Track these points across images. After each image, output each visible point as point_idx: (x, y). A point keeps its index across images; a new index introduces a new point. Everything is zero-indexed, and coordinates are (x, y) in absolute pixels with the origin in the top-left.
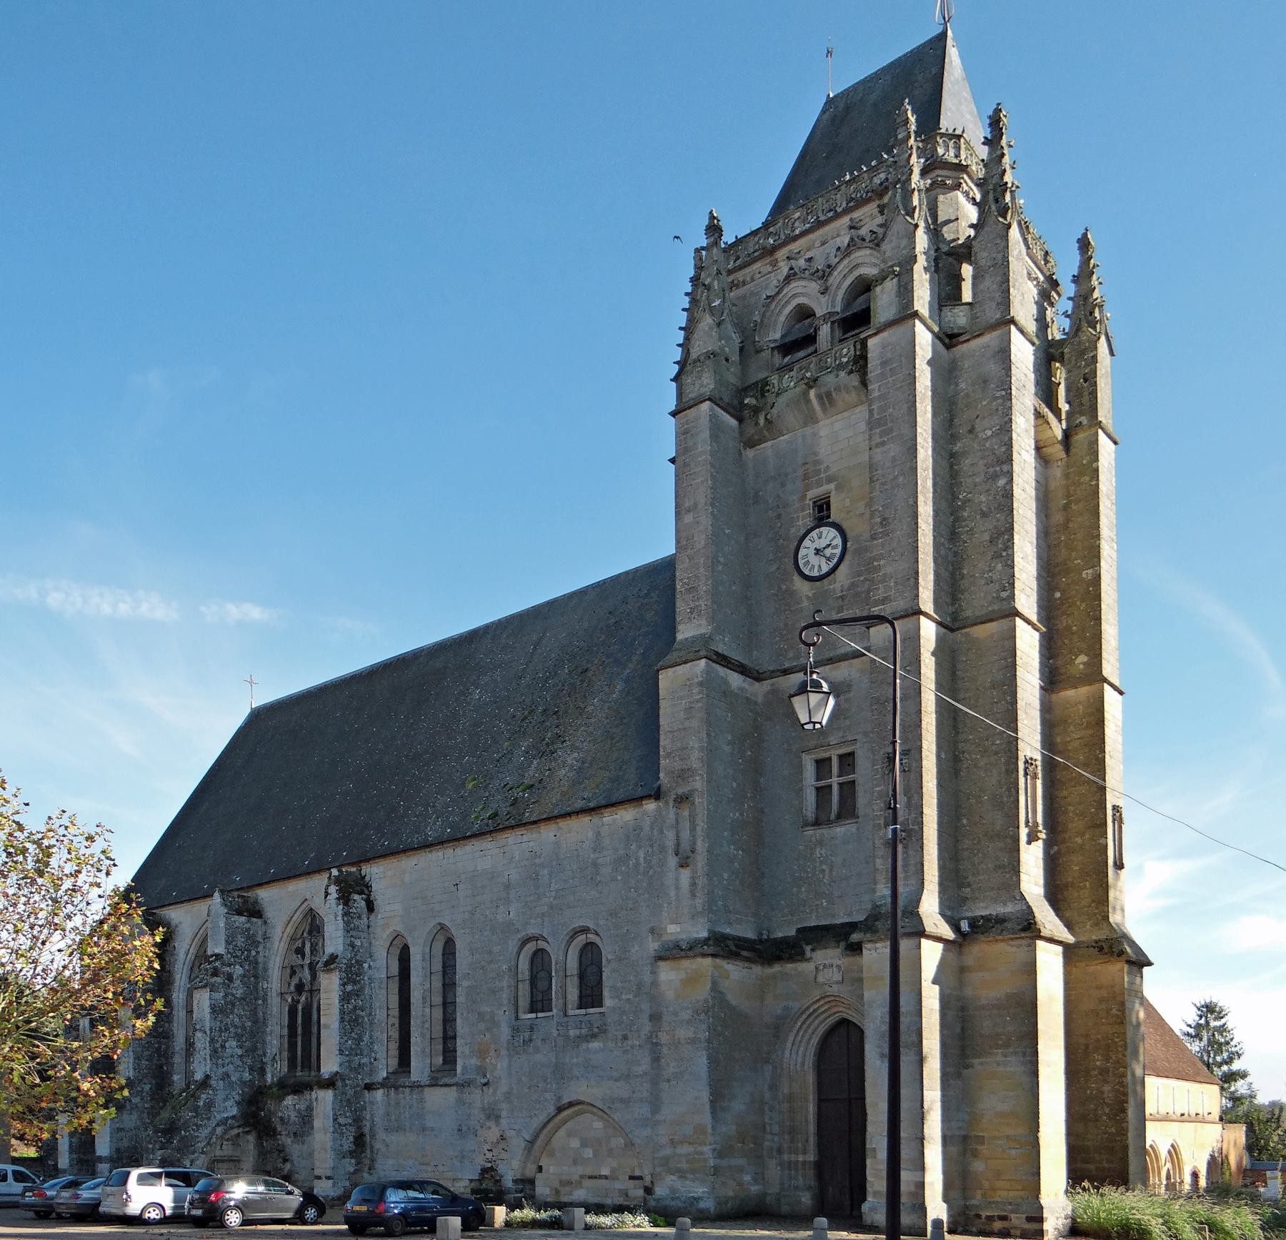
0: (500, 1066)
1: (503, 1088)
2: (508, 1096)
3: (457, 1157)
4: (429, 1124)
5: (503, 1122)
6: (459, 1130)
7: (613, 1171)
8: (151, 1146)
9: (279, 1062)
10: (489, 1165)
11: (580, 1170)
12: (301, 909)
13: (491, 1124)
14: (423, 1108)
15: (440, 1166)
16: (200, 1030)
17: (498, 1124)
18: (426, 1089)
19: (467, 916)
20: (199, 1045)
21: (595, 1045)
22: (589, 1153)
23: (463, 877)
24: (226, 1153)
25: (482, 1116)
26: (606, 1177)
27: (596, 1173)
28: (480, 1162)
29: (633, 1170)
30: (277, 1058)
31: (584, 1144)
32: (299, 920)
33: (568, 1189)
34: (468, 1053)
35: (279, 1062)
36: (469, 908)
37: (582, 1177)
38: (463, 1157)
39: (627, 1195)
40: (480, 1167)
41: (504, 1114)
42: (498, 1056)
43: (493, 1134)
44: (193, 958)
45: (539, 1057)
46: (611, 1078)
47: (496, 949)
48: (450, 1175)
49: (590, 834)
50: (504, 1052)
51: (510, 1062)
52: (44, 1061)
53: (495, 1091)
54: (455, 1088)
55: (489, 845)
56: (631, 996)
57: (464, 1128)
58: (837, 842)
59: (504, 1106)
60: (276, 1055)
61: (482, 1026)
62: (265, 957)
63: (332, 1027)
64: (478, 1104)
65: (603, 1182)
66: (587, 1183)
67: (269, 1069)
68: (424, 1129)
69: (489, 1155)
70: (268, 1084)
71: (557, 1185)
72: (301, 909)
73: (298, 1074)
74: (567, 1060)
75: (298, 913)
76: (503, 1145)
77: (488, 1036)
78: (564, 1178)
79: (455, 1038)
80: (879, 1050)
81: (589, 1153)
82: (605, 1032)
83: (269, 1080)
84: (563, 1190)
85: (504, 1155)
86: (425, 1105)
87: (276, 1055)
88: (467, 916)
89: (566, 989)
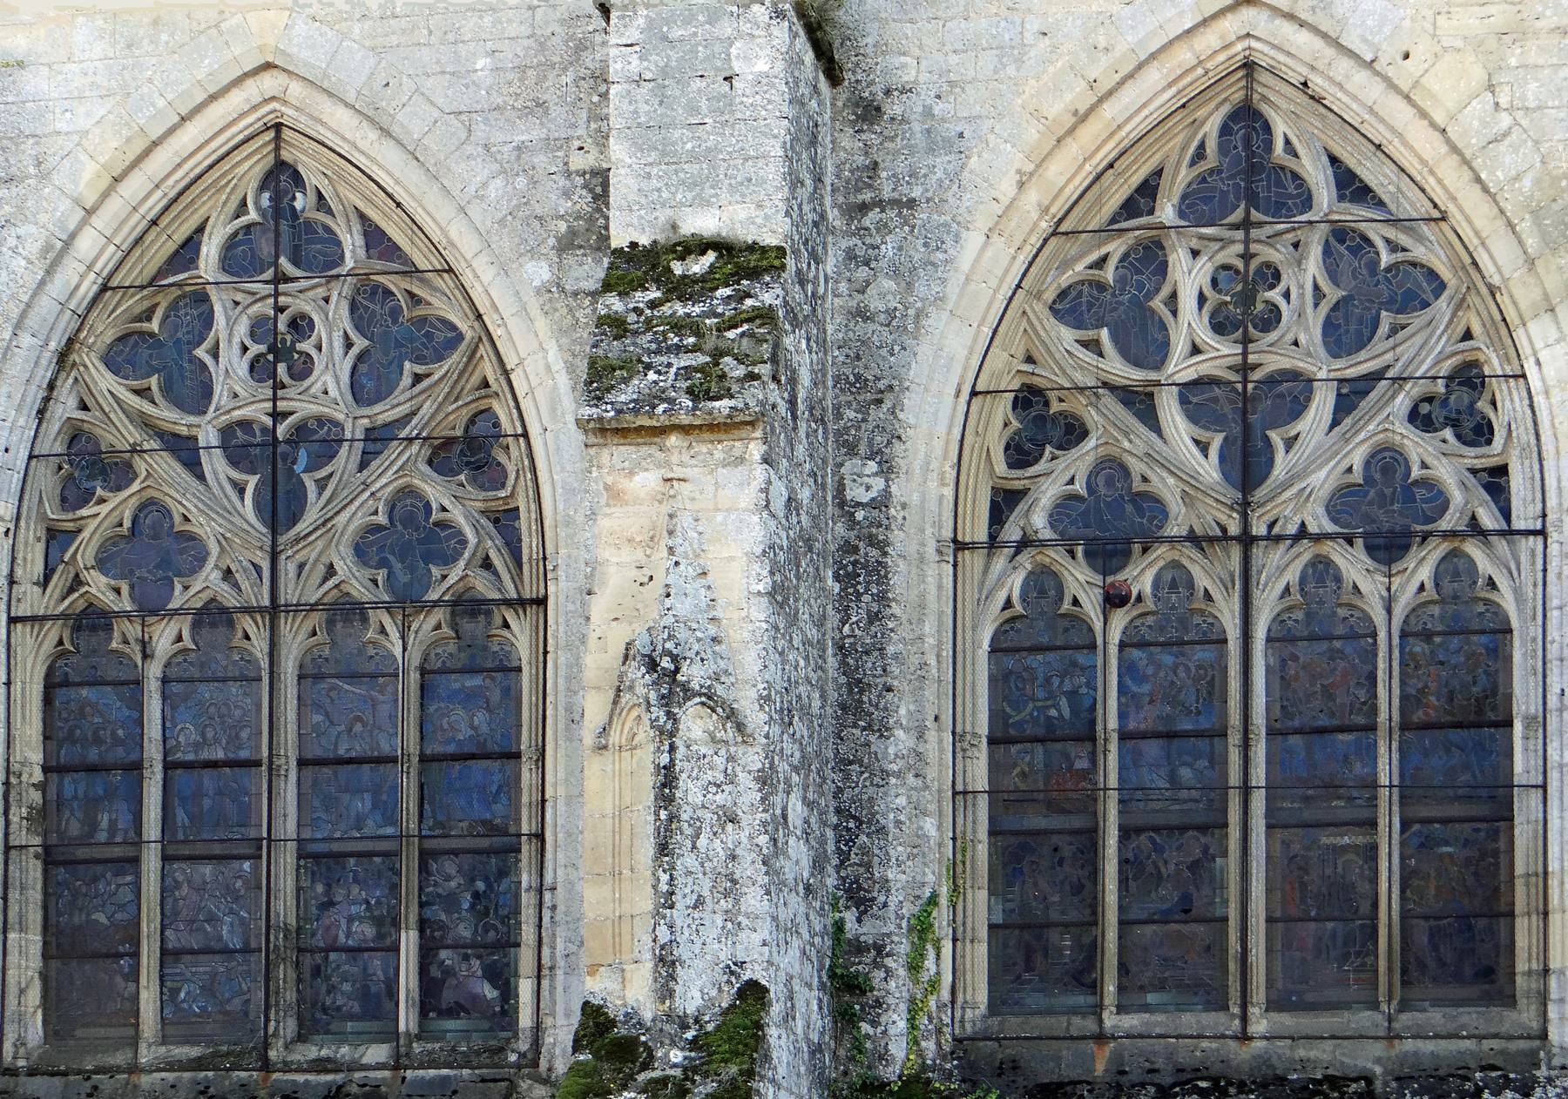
9: (947, 947)
12: (1184, 56)
16: (710, 700)
20: (696, 796)
30: (941, 918)
32: (1154, 111)
35: (947, 947)
44: (89, 287)
52: (741, 405)
60: (933, 900)
62: (862, 314)
67: (895, 987)
70: (890, 1073)
72: (1184, 56)
73: (1110, 1020)
75: (1154, 77)
79: (519, 945)
80: (870, 998)
83: (898, 1049)
87: (933, 900)
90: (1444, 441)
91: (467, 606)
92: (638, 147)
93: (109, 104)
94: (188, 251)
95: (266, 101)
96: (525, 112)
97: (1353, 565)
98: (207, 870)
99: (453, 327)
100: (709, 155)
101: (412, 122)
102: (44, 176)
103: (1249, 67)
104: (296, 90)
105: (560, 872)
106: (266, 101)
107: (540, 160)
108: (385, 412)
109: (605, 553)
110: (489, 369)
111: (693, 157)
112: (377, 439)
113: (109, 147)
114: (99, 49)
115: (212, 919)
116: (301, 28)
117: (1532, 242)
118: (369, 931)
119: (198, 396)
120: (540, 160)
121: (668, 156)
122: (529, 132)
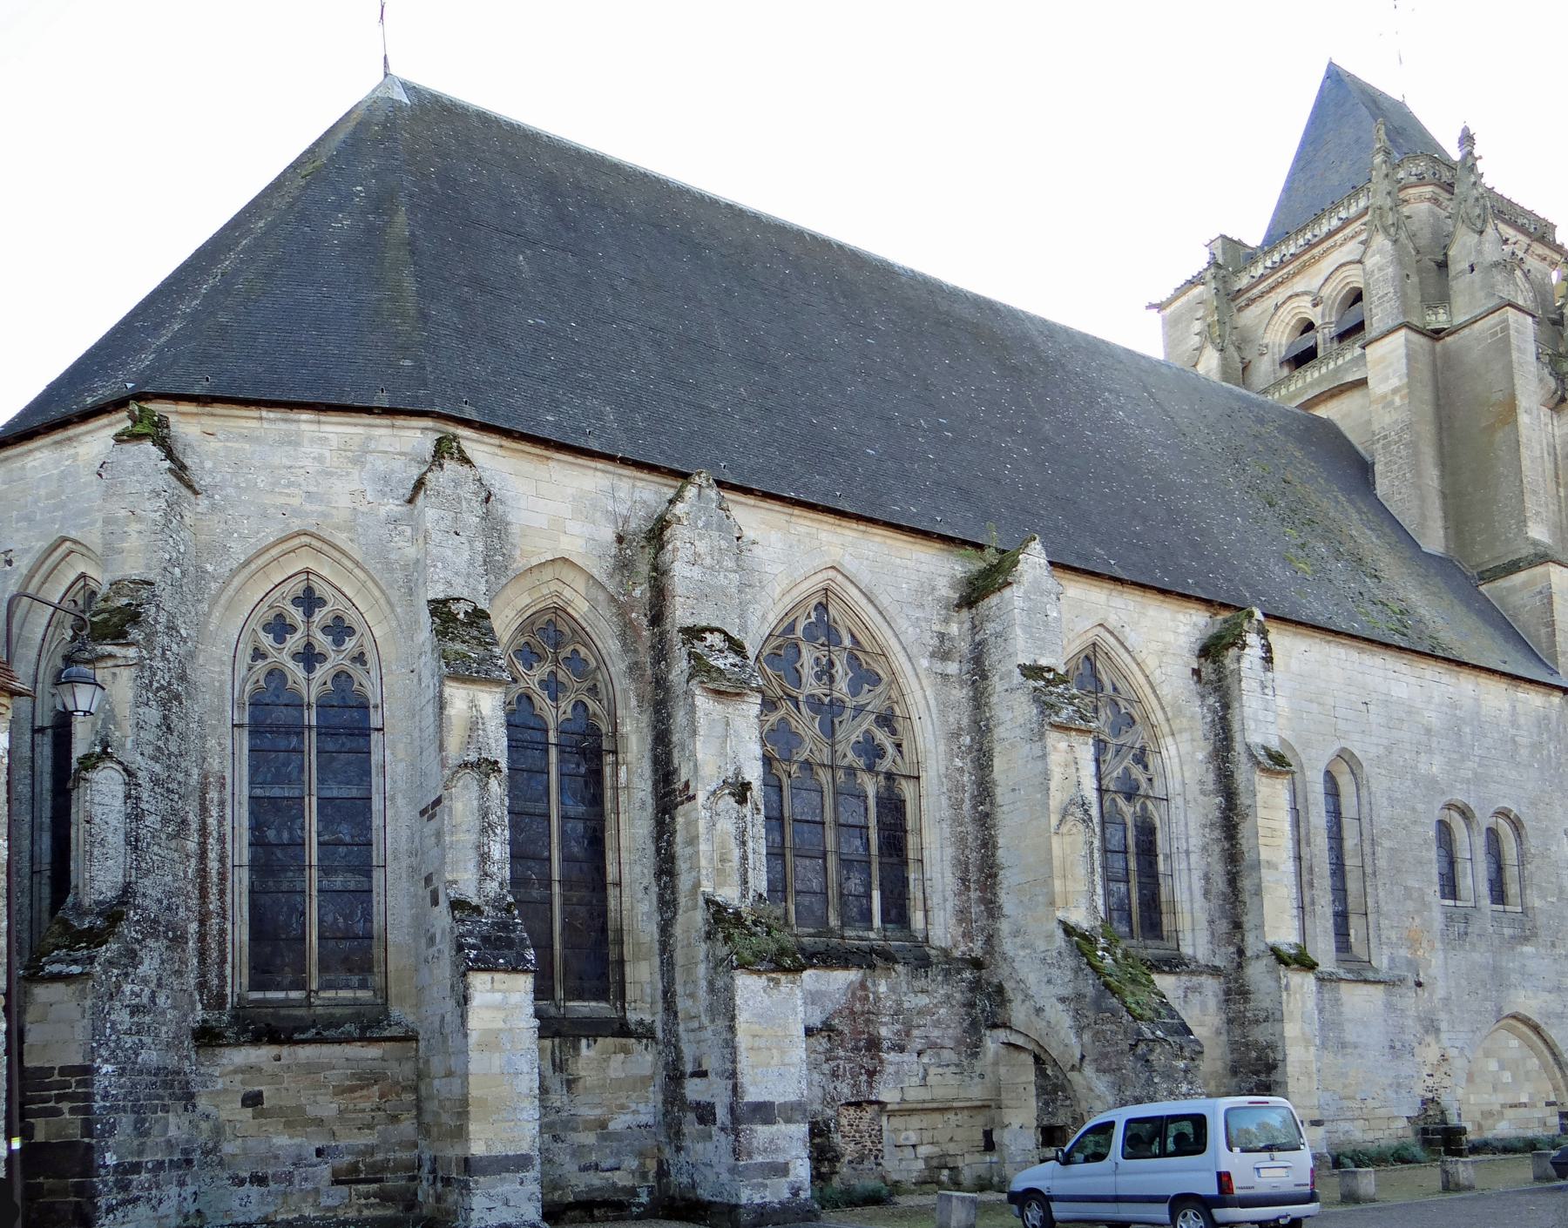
0: (1435, 963)
1: (1440, 993)
2: (1446, 1000)
3: (1391, 1085)
4: (1350, 1037)
5: (1444, 1036)
6: (1392, 1047)
7: (1531, 1096)
8: (1181, 1064)
10: (1430, 1095)
11: (1501, 1098)
13: (1430, 1039)
14: (1340, 1014)
15: (1370, 1100)
17: (1438, 1040)
18: (1343, 985)
19: (1381, 751)
21: (1528, 949)
22: (1507, 1077)
23: (1374, 695)
24: (939, 1093)
25: (1418, 1027)
26: (1525, 1105)
27: (1516, 1101)
28: (1420, 1091)
29: (1548, 1095)
31: (1502, 1067)
33: (1490, 1122)
34: (1394, 939)
36: (1385, 742)
37: (1503, 1106)
38: (1399, 1085)
39: (1545, 1124)
40: (1420, 1099)
41: (1444, 1026)
42: (1433, 948)
43: (1431, 1054)
45: (1476, 956)
46: (1544, 990)
47: (1420, 807)
48: (1382, 1112)
49: (1507, 705)
50: (1438, 945)
51: (1445, 958)
53: (1431, 995)
54: (1381, 987)
55: (1404, 669)
56: (1554, 899)
57: (1398, 1045)
58: (686, 735)
59: (1443, 1016)
61: (1410, 905)
63: (1282, 868)
64: (1412, 1012)
65: (1522, 1110)
66: (1510, 1113)
68: (1344, 1045)
69: (1430, 1082)
71: (1478, 1117)
74: (1504, 964)
76: (1445, 1068)
77: (1418, 920)
78: (1486, 1108)
81: (1507, 1077)
82: (1536, 935)
84: (1487, 1123)
85: (1447, 1082)
86: (1343, 1009)
88: (1381, 751)
89: (1474, 877)
90: (845, 756)
91: (890, 776)
92: (1025, 632)
93: (784, 566)
94: (791, 628)
95: (298, 534)
96: (918, 607)
97: (1121, 802)
98: (807, 862)
99: (878, 675)
100: (1044, 639)
101: (884, 600)
102: (762, 588)
103: (1094, 644)
104: (840, 578)
105: (625, 869)
106: (298, 534)
107: (923, 624)
108: (862, 699)
109: (1054, 768)
110: (894, 694)
111: (1039, 639)
112: (859, 710)
113: (785, 583)
114: (780, 545)
115: (810, 880)
116: (847, 557)
117: (1170, 715)
118: (862, 890)
119: (798, 682)
120: (923, 624)
121: (1032, 637)
122: (919, 614)
